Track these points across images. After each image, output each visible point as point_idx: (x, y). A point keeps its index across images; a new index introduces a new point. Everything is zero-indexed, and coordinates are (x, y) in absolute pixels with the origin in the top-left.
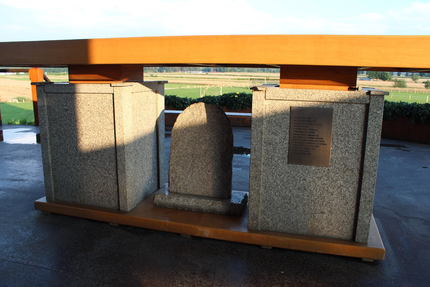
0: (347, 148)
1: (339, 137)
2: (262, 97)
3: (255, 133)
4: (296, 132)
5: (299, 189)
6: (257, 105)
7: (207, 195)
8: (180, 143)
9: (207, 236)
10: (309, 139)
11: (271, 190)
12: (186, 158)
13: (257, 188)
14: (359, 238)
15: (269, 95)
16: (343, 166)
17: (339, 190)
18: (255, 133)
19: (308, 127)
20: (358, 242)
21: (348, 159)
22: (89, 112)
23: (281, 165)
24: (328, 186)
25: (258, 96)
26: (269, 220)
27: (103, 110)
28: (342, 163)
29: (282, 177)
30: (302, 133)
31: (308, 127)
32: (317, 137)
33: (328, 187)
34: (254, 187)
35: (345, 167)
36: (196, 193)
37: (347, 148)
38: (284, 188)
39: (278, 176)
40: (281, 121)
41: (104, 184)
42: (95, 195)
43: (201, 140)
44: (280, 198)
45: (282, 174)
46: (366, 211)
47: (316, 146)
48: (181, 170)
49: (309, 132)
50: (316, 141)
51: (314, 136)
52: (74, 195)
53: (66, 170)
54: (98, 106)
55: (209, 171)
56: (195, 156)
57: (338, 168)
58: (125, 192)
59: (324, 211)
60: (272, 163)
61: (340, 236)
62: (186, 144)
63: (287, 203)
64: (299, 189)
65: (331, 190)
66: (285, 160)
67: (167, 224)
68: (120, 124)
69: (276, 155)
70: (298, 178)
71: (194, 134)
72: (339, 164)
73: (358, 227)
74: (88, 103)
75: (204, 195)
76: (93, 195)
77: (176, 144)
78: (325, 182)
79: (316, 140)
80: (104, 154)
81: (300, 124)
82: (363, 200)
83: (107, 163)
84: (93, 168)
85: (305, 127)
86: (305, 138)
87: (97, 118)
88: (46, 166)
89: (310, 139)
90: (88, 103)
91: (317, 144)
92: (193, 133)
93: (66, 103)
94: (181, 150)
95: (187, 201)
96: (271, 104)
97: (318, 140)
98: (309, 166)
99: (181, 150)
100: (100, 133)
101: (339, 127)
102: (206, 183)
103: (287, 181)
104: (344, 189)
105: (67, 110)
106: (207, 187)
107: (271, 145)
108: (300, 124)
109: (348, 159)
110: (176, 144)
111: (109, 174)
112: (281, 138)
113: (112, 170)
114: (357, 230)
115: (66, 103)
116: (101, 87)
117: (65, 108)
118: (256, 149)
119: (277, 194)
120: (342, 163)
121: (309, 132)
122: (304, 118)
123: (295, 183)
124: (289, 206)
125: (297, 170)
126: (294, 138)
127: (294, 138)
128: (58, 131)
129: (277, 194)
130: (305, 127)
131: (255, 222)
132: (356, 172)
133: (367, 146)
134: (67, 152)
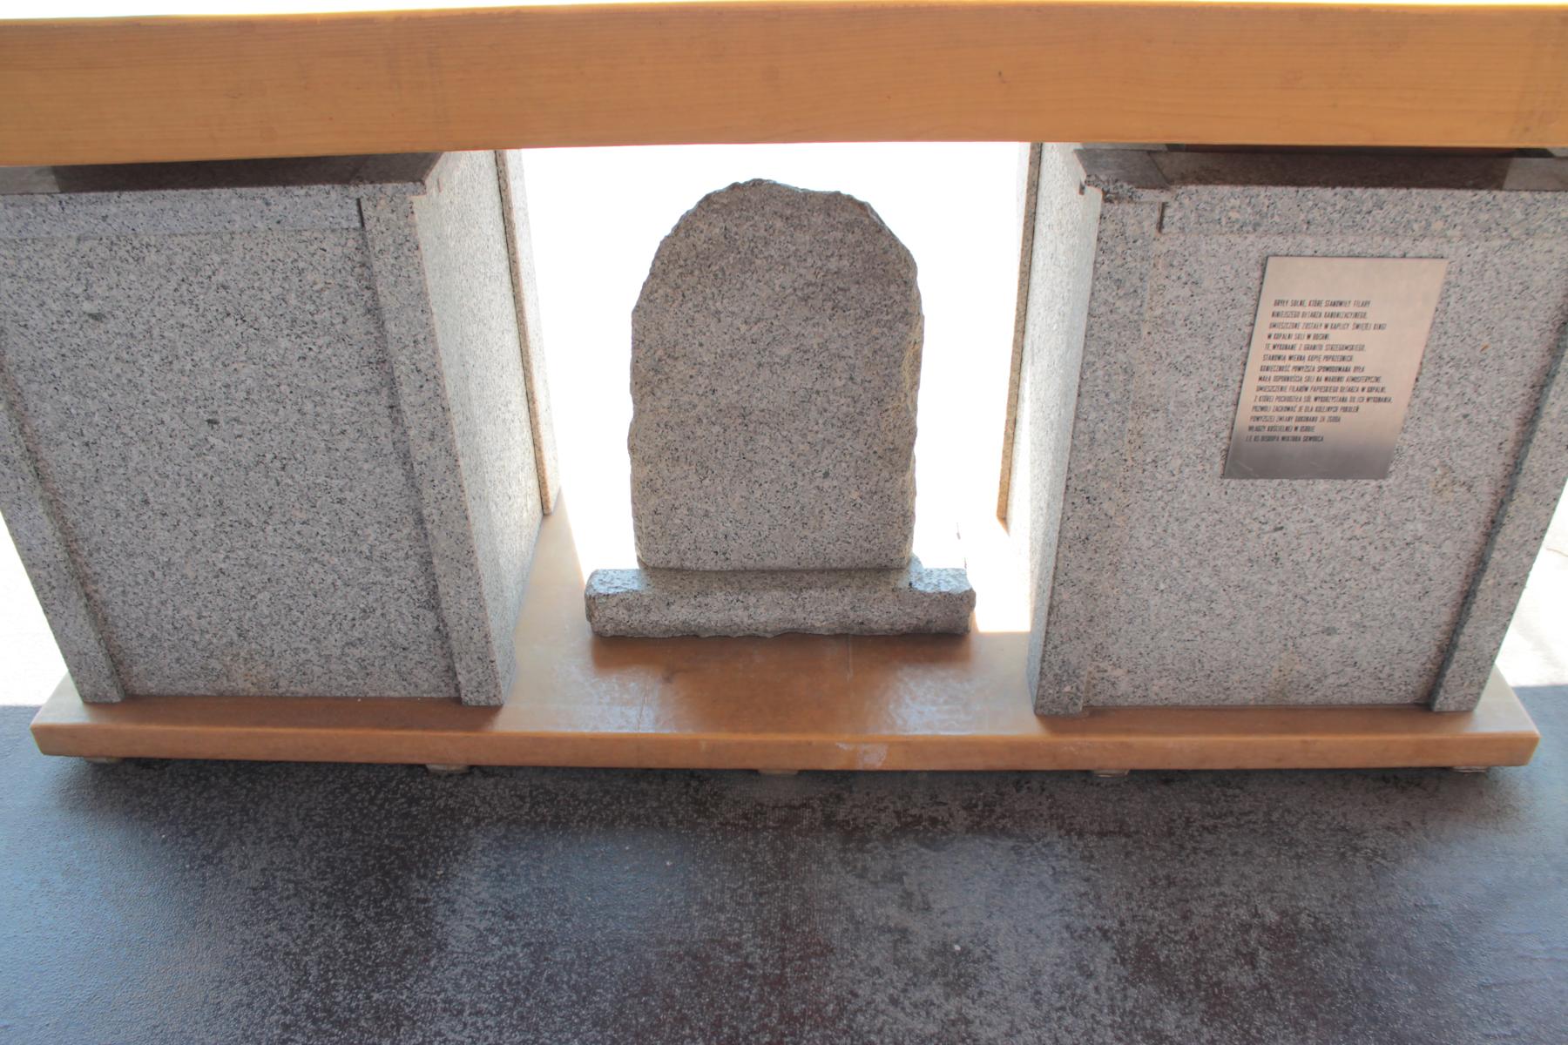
0: (1469, 409)
1: (1446, 369)
2: (1146, 224)
3: (1100, 373)
4: (1272, 358)
5: (1250, 560)
6: (1119, 262)
7: (818, 564)
8: (680, 366)
9: (878, 766)
10: (1323, 383)
11: (1141, 573)
12: (716, 429)
13: (1088, 578)
14: (1443, 702)
15: (1179, 215)
16: (1439, 472)
17: (1405, 555)
18: (1100, 373)
19: (1326, 337)
20: (1440, 713)
21: (1461, 445)
22: (230, 321)
23: (1191, 483)
24: (1366, 543)
25: (1130, 221)
26: (1118, 672)
27: (310, 307)
28: (1435, 462)
29: (1189, 526)
30: (1300, 363)
31: (1326, 337)
32: (1357, 374)
33: (1364, 548)
34: (1073, 576)
35: (1443, 476)
36: (769, 562)
37: (1469, 409)
38: (1193, 562)
39: (1174, 526)
40: (1214, 318)
41: (366, 612)
42: (328, 657)
43: (784, 352)
44: (1173, 598)
45: (1192, 514)
46: (1492, 616)
47: (1345, 409)
48: (693, 478)
49: (1327, 358)
50: (1351, 390)
51: (1347, 370)
52: (219, 667)
53: (158, 574)
54: (277, 291)
55: (826, 475)
56: (753, 418)
57: (1418, 480)
58: (477, 636)
59: (1337, 625)
60: (1153, 477)
61: (1383, 697)
62: (706, 371)
63: (1197, 611)
64: (1250, 560)
65: (1375, 557)
66: (1213, 464)
67: (703, 746)
68: (422, 366)
69: (1176, 448)
70: (1255, 526)
71: (744, 328)
72: (1425, 465)
73: (1454, 666)
74: (220, 278)
75: (804, 564)
76: (315, 659)
77: (657, 372)
78: (1358, 532)
79: (1352, 384)
80: (348, 495)
81: (1296, 326)
82: (1490, 582)
83: (369, 531)
84: (298, 556)
85: (1316, 337)
86: (1308, 379)
87: (284, 343)
88: (44, 573)
89: (1329, 384)
90: (220, 278)
91: (1353, 399)
92: (738, 322)
93: (88, 285)
94: (686, 398)
95: (747, 608)
96: (1180, 250)
97: (1360, 385)
98: (1304, 482)
99: (686, 398)
100: (309, 407)
101: (1451, 331)
102: (812, 522)
103: (1211, 539)
104: (1426, 548)
105: (97, 317)
106: (817, 535)
107: (1159, 415)
108: (1296, 326)
109: (1461, 445)
110: (657, 372)
111: (388, 572)
112: (1204, 385)
113: (401, 554)
114: (1449, 673)
115: (88, 285)
116: (286, 201)
117: (88, 307)
118: (1098, 436)
119: (1162, 586)
120: (1435, 462)
121: (1327, 358)
122: (1318, 303)
123: (1238, 544)
124: (1203, 621)
125: (1254, 498)
126: (1262, 384)
127: (1262, 384)
128: (71, 416)
129: (1162, 586)
130: (1316, 337)
131: (1067, 689)
132: (1485, 492)
133: (1552, 400)
134: (146, 502)
